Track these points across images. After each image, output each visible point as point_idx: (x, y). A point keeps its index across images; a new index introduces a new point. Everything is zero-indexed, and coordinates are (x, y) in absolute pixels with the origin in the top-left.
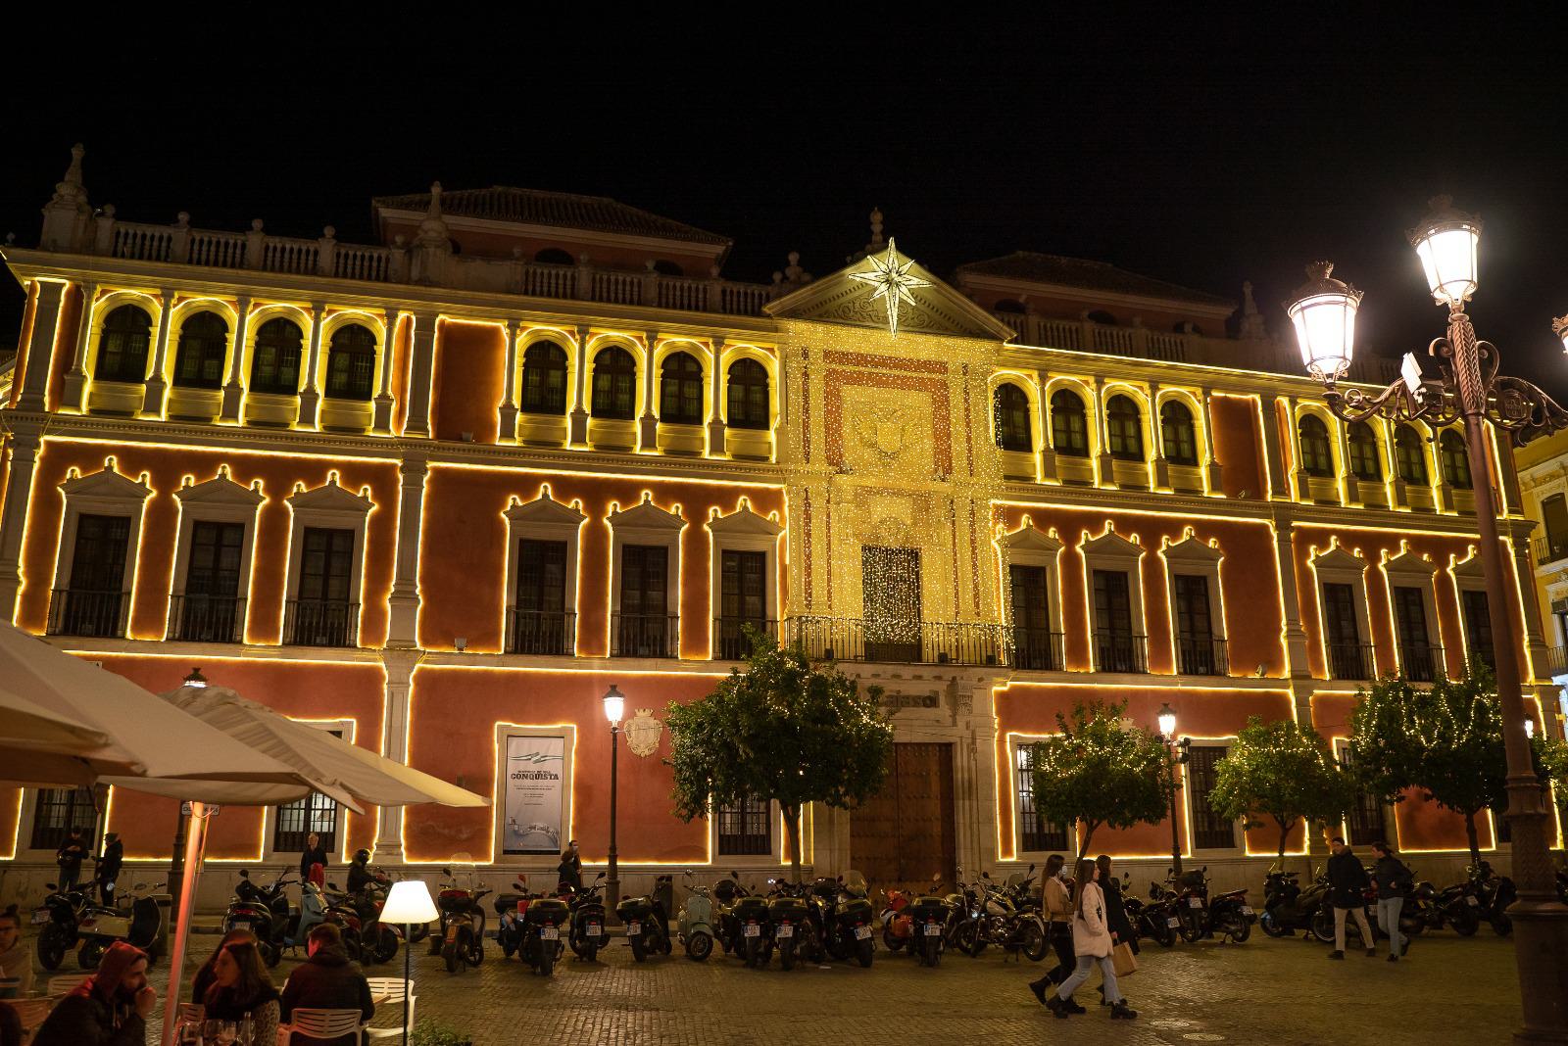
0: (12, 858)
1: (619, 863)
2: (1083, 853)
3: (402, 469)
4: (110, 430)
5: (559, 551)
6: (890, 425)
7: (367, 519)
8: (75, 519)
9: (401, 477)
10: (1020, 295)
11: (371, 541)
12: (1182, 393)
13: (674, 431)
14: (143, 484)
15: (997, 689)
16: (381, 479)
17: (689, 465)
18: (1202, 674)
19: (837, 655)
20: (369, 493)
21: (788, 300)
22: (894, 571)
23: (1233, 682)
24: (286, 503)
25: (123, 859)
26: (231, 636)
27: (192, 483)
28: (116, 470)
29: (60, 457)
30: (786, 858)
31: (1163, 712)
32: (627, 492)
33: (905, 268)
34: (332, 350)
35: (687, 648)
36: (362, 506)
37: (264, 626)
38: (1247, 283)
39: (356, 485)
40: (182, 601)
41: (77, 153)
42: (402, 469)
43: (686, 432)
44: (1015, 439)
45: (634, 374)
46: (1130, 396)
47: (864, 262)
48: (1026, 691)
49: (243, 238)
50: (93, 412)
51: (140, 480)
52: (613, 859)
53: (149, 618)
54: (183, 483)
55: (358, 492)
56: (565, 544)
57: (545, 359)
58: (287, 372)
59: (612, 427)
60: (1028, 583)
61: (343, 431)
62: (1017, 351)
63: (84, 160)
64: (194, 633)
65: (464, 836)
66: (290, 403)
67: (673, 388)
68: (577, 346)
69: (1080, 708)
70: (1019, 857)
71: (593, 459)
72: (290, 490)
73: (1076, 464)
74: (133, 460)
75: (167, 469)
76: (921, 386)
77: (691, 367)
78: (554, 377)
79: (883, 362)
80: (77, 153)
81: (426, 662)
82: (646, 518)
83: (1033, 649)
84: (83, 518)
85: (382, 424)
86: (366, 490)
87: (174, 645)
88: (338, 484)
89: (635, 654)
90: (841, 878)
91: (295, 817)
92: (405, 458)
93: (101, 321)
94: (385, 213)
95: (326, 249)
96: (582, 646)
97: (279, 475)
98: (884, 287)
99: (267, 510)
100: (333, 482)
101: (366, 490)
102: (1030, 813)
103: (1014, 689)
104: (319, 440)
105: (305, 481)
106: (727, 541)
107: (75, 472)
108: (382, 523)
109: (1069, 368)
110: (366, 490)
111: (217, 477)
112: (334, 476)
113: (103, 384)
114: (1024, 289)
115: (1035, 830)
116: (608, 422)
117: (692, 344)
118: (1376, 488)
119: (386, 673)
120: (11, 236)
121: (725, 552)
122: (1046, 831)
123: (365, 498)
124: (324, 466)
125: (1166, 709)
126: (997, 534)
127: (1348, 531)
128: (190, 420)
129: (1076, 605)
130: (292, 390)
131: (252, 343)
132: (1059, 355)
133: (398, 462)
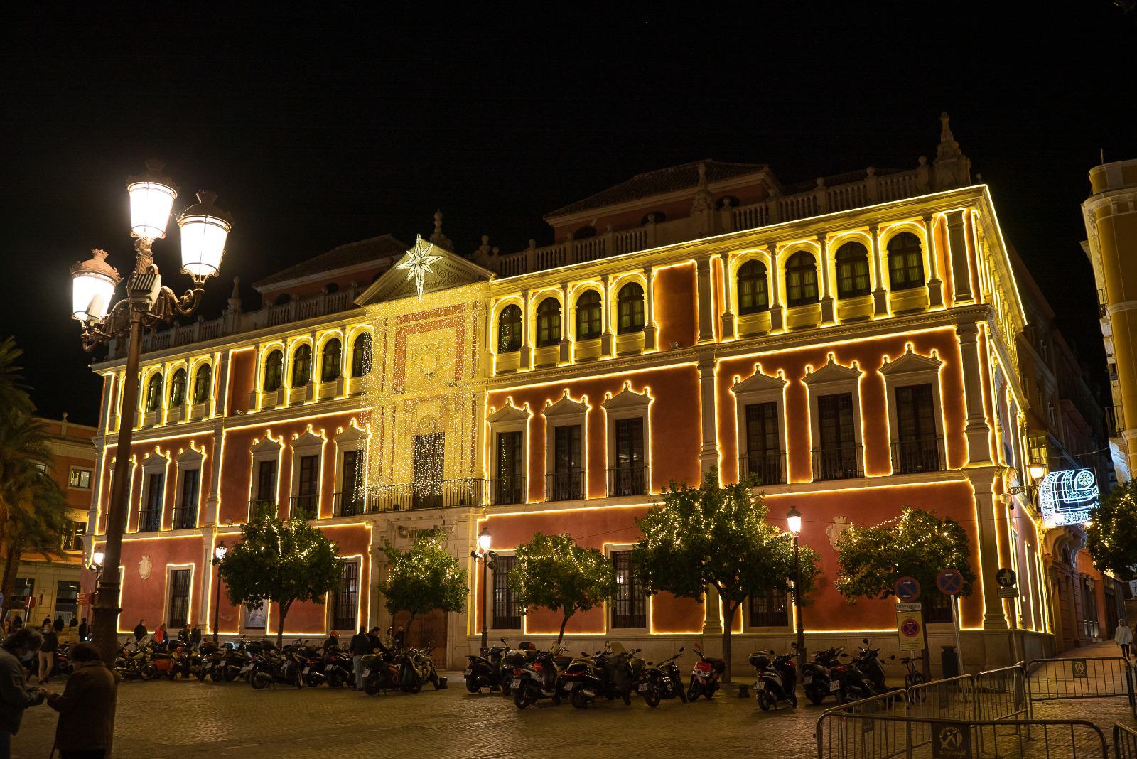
0: (118, 631)
1: (805, 632)
2: (800, 628)
3: (958, 332)
4: (852, 333)
5: (847, 401)
6: (431, 354)
7: (784, 389)
8: (743, 410)
9: (958, 338)
10: (591, 221)
11: (204, 474)
12: (554, 291)
13: (851, 304)
14: (780, 378)
15: (479, 520)
16: (944, 343)
17: (916, 320)
18: (628, 495)
19: (467, 502)
20: (937, 355)
21: (367, 293)
22: (428, 449)
23: (871, 482)
24: (879, 372)
25: (732, 633)
26: (779, 480)
27: (889, 361)
28: (836, 362)
29: (728, 370)
30: (478, 631)
31: (790, 515)
32: (817, 357)
33: (412, 256)
34: (787, 274)
35: (795, 475)
36: (934, 365)
37: (878, 462)
38: (944, 113)
39: (927, 351)
40: (898, 446)
41: (945, 121)
42: (958, 332)
43: (808, 310)
44: (511, 343)
45: (920, 250)
46: (594, 289)
47: (406, 256)
48: (499, 519)
49: (813, 194)
50: (744, 336)
51: (777, 377)
52: (280, 632)
53: (800, 470)
54: (883, 362)
55: (930, 355)
56: (642, 418)
57: (752, 273)
58: (760, 298)
59: (855, 303)
60: (507, 445)
61: (909, 313)
62: (502, 283)
63: (950, 123)
64: (775, 480)
65: (230, 620)
66: (865, 302)
67: (899, 263)
68: (925, 231)
69: (539, 531)
70: (744, 631)
71: (742, 345)
72: (880, 363)
73: (550, 351)
74: (771, 364)
75: (793, 365)
76: (450, 323)
77: (807, 261)
78: (913, 260)
79: (423, 316)
80: (945, 121)
81: (219, 532)
82: (911, 364)
83: (508, 492)
84: (303, 459)
85: (936, 301)
86: (934, 352)
87: (337, 520)
88: (914, 352)
89: (911, 471)
90: (793, 644)
91: (623, 605)
92: (959, 323)
93: (535, 311)
94: (259, 289)
95: (871, 183)
96: (591, 493)
97: (869, 355)
98: (424, 267)
99: (790, 390)
100: (910, 351)
101: (934, 353)
102: (625, 600)
103: (492, 519)
104: (894, 323)
105: (888, 353)
106: (557, 421)
107: (738, 379)
108: (951, 374)
109: (540, 284)
110: (934, 353)
111: (905, 353)
112: (910, 347)
113: (581, 343)
114: (591, 216)
115: (505, 615)
116: (750, 316)
117: (757, 253)
118: (913, 294)
119: (972, 487)
120: (94, 359)
121: (346, 453)
122: (513, 615)
123: (935, 358)
124: (750, 362)
125: (794, 512)
126: (488, 410)
127: (165, 441)
128: (803, 329)
129: (541, 453)
130: (867, 291)
131: (534, 318)
132: (907, 204)
133: (696, 364)
